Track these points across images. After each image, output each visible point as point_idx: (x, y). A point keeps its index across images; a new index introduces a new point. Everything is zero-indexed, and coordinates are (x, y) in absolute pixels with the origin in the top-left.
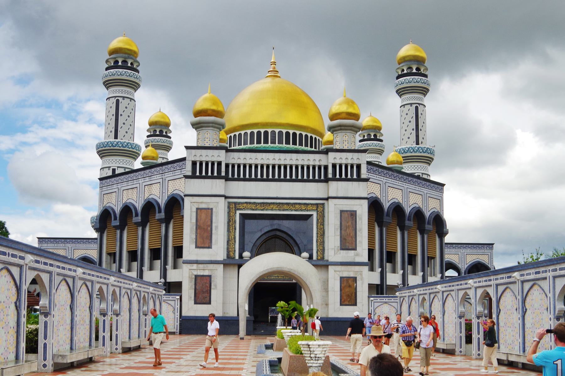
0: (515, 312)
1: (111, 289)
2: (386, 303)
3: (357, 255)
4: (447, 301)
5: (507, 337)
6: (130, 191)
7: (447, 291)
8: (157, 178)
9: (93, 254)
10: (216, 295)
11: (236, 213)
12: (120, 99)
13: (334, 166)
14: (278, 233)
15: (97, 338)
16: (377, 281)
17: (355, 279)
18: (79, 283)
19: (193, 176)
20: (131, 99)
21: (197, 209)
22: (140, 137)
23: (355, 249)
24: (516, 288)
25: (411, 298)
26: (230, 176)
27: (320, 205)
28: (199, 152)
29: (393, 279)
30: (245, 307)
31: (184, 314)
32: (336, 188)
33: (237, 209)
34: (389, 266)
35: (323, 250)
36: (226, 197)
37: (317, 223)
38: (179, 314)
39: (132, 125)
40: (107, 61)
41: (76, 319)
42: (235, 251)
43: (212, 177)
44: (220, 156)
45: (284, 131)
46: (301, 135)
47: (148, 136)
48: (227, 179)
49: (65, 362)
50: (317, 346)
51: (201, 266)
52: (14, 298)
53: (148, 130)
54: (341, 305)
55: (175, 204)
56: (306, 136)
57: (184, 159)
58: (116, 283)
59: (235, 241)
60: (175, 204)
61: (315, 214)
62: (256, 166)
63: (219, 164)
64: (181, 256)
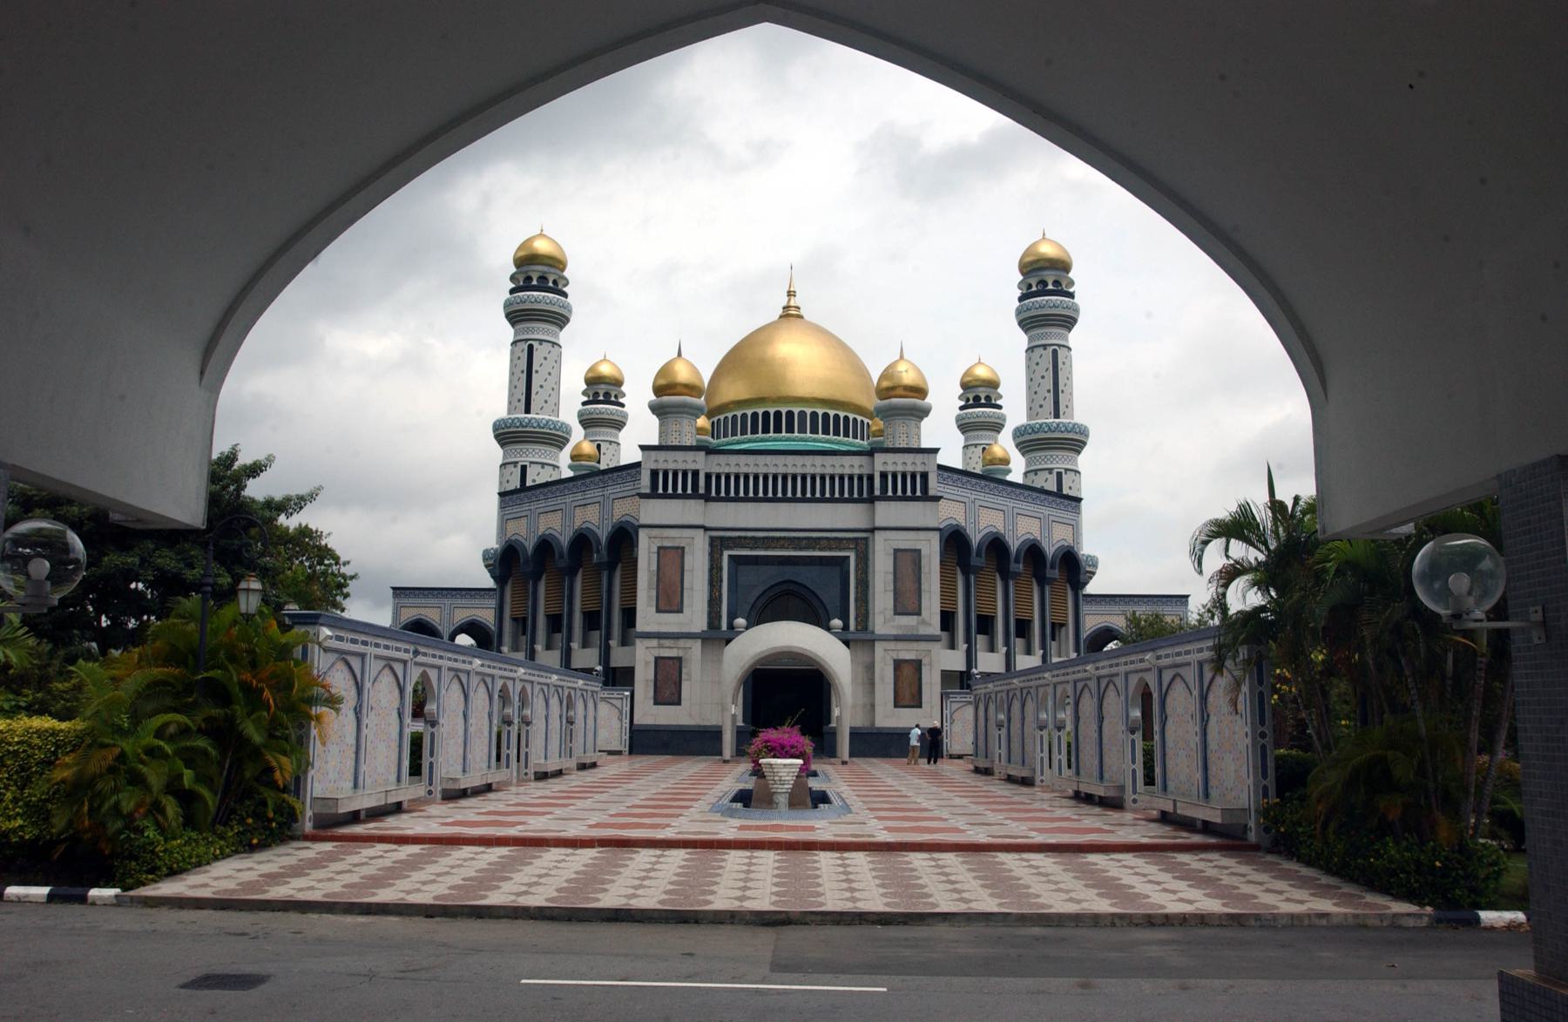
1: (519, 686)
8: (594, 494)
9: (486, 614)
12: (536, 344)
13: (884, 475)
14: (792, 587)
15: (498, 758)
16: (960, 665)
18: (475, 680)
19: (653, 495)
20: (554, 344)
22: (569, 402)
26: (713, 494)
27: (862, 543)
28: (662, 455)
29: (989, 662)
30: (736, 710)
32: (887, 513)
34: (981, 640)
39: (556, 388)
41: (471, 729)
43: (684, 496)
44: (699, 462)
45: (808, 411)
46: (837, 417)
47: (584, 404)
48: (707, 498)
51: (667, 643)
52: (396, 704)
53: (584, 393)
54: (896, 706)
55: (624, 538)
56: (846, 418)
57: (637, 465)
61: (852, 556)
62: (756, 477)
63: (696, 473)
64: (634, 626)
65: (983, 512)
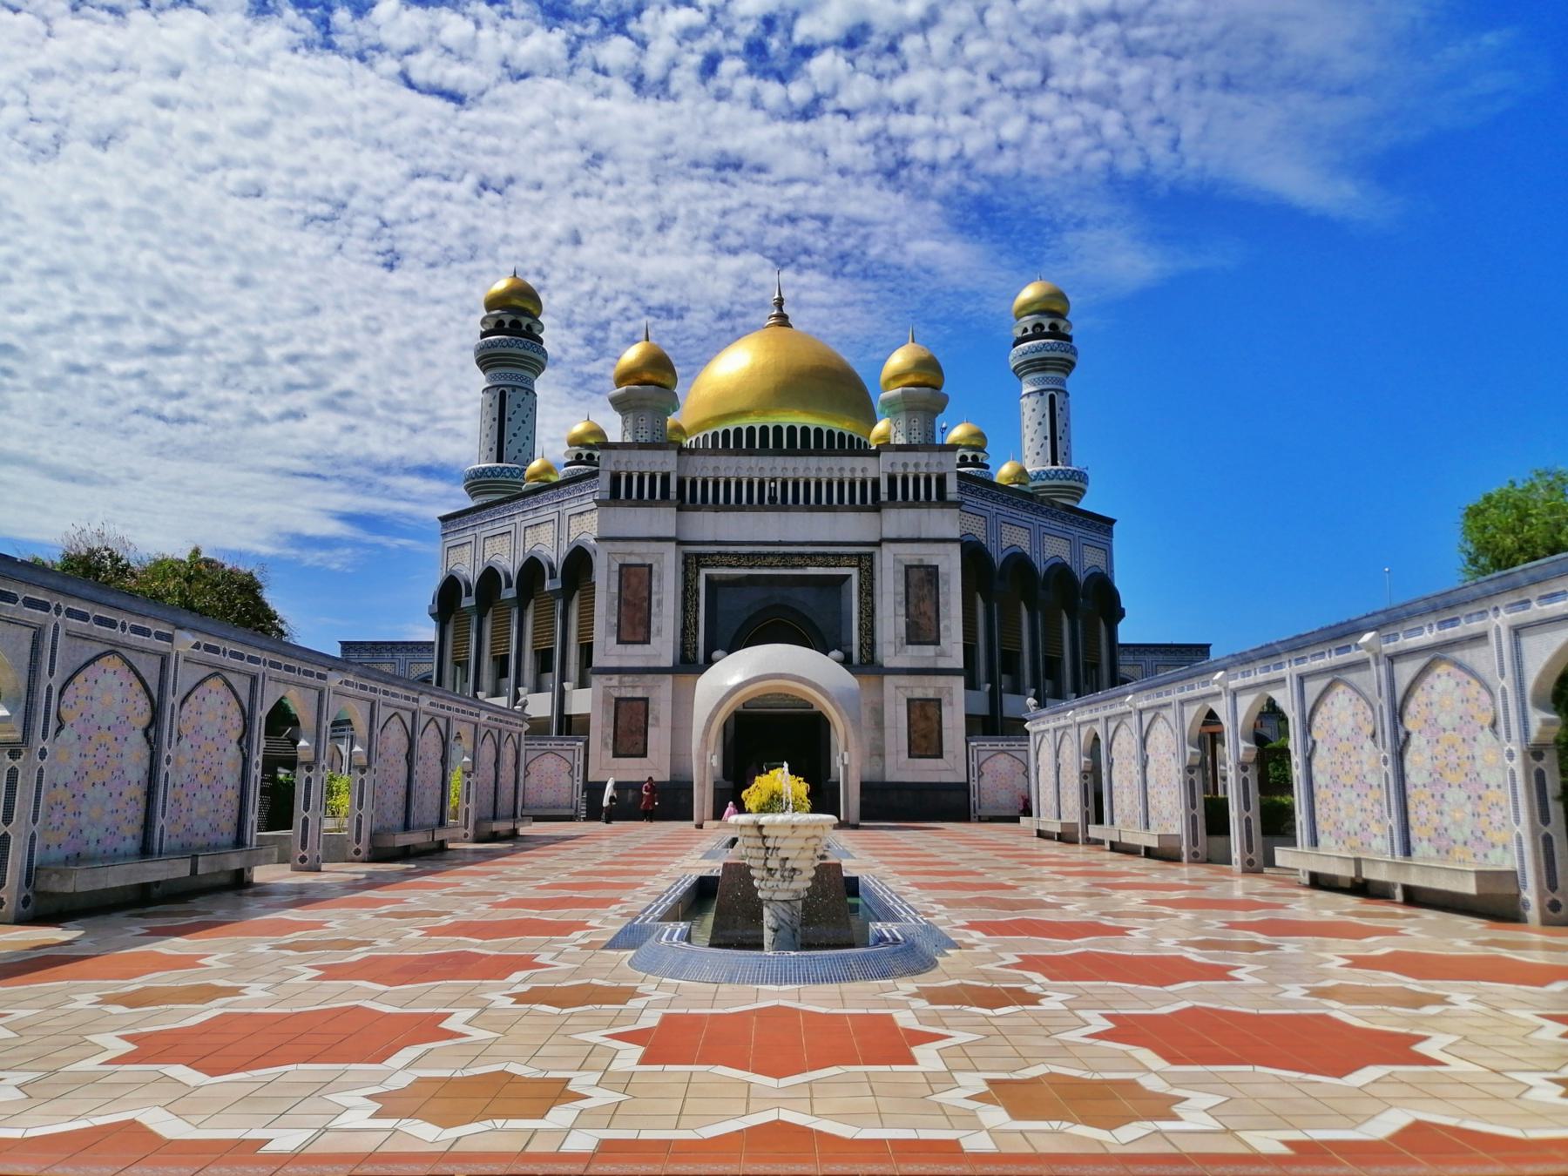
0: (1369, 744)
2: (1003, 752)
3: (941, 655)
4: (1152, 732)
5: (1343, 814)
6: (497, 540)
7: (1152, 708)
10: (658, 737)
11: (698, 574)
17: (938, 702)
21: (622, 566)
23: (937, 642)
24: (1370, 680)
25: (1059, 734)
31: (590, 779)
32: (897, 521)
33: (700, 565)
35: (872, 645)
36: (680, 543)
37: (860, 593)
38: (581, 777)
40: (483, 322)
42: (696, 648)
49: (69, 888)
50: (788, 832)
51: (628, 679)
58: (492, 723)
59: (697, 630)
60: (579, 562)
61: (854, 572)
63: (666, 478)
65: (1006, 528)
